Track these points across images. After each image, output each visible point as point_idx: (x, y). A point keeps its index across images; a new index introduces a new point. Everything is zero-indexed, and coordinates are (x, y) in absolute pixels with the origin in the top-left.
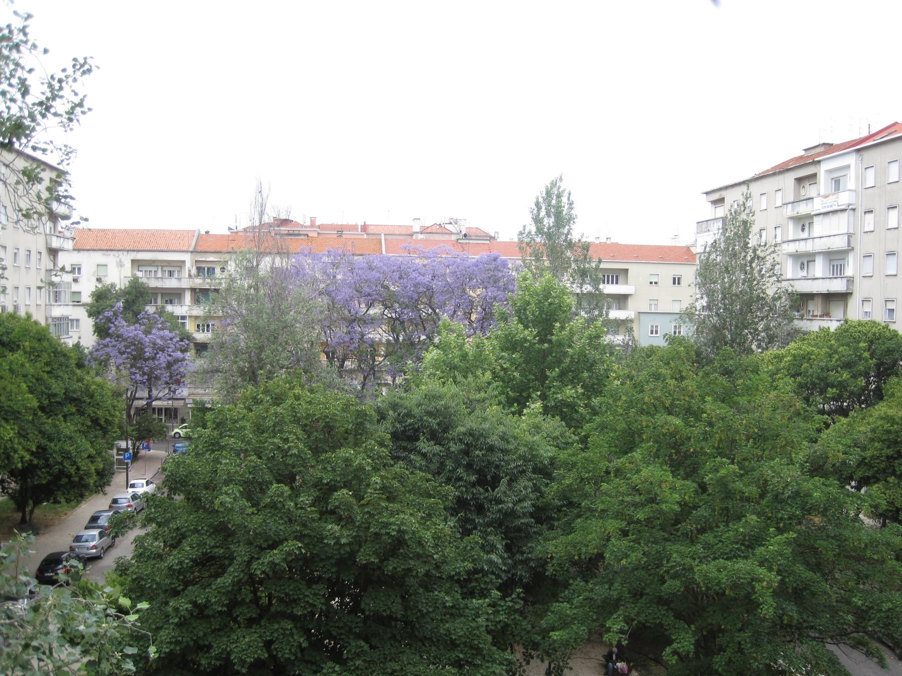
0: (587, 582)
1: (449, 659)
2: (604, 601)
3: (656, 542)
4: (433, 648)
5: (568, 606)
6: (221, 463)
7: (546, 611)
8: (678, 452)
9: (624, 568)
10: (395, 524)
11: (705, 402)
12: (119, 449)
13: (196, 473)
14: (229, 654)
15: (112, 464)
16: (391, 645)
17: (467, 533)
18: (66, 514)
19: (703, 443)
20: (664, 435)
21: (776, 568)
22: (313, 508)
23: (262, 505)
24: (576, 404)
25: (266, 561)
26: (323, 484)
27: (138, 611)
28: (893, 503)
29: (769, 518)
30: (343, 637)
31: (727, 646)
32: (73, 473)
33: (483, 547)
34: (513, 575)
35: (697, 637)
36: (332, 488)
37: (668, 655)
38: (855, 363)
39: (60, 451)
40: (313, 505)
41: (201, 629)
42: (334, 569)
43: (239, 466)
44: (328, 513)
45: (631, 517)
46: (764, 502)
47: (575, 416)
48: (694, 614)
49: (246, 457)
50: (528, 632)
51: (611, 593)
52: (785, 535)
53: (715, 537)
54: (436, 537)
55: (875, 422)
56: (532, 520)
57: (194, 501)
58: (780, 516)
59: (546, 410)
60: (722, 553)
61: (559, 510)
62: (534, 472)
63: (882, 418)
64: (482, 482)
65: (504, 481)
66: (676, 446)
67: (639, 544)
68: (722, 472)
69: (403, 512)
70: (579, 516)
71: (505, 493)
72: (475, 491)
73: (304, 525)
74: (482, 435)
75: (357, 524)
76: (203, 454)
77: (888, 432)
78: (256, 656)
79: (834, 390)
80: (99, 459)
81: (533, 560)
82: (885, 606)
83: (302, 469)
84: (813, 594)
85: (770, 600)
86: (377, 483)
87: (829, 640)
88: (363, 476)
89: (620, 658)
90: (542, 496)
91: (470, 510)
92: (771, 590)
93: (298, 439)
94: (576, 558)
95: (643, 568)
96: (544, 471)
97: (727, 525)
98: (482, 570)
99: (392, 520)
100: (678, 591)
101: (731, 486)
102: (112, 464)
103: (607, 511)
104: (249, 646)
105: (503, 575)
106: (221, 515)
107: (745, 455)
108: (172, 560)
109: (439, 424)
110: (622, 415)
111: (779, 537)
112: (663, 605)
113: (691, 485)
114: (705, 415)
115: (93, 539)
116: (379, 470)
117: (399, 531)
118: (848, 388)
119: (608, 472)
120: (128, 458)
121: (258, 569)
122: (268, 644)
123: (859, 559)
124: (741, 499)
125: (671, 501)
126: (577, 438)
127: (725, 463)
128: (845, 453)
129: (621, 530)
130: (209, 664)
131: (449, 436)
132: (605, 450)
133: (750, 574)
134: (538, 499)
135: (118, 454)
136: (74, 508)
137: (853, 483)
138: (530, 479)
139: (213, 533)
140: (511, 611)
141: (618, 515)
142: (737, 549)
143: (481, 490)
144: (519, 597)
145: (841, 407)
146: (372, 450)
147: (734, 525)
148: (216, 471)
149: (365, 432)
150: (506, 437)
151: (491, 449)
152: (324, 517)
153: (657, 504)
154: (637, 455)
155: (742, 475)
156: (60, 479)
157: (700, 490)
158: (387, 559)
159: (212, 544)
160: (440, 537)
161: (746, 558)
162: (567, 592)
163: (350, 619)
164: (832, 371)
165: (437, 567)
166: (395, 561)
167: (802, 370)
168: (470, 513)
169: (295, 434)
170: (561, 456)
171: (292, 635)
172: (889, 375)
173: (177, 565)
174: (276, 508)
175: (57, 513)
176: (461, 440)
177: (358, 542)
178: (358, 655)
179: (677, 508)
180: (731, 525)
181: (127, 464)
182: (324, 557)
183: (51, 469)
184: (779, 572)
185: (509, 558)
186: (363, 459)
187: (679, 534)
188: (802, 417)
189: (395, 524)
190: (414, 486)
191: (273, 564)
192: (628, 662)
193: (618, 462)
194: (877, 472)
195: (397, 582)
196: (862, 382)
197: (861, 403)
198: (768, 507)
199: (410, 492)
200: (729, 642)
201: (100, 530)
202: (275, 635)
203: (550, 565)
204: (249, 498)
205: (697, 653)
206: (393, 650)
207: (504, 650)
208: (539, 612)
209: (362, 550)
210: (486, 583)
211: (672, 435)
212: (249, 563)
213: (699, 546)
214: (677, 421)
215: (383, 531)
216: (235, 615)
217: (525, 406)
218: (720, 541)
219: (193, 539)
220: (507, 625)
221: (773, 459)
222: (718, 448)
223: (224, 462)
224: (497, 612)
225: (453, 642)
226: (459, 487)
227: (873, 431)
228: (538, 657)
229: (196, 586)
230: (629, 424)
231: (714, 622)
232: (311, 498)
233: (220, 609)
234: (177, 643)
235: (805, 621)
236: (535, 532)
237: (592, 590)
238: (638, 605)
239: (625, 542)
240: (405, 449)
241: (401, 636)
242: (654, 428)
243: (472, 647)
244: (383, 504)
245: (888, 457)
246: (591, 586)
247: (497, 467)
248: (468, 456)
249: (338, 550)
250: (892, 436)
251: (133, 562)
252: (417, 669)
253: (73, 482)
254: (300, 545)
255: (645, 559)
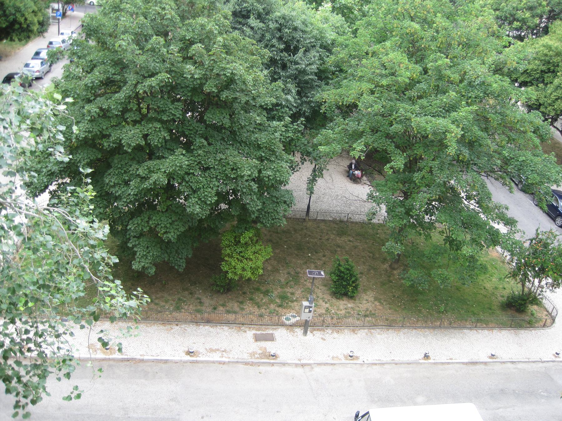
0: (344, 119)
1: (256, 156)
2: (354, 132)
3: (391, 100)
4: (247, 148)
5: (332, 132)
6: (121, 20)
7: (317, 134)
8: (414, 46)
9: (370, 113)
10: (230, 69)
11: (436, 17)
12: (53, 9)
13: (104, 26)
14: (120, 141)
15: (49, 18)
16: (221, 144)
17: (274, 80)
18: (19, 49)
19: (431, 43)
20: (407, 34)
21: (461, 126)
22: (179, 54)
23: (146, 49)
24: (352, 8)
25: (147, 84)
26: (186, 40)
27: (66, 104)
28: (538, 100)
29: (463, 96)
30: (192, 136)
31: (424, 168)
32: (23, 22)
33: (283, 90)
34: (300, 110)
35: (406, 161)
36: (192, 43)
37: (388, 169)
38: (535, 8)
39: (13, 6)
40: (179, 52)
41: (105, 124)
42: (189, 94)
43: (133, 23)
44: (187, 58)
45: (378, 83)
46: (461, 85)
47: (351, 16)
48: (406, 147)
49: (137, 17)
50: (305, 145)
51: (359, 127)
52: (471, 107)
53: (428, 102)
54: (255, 80)
55: (539, 48)
56: (316, 78)
57: (102, 44)
58: (470, 95)
59: (334, 9)
60: (430, 113)
61: (333, 74)
62: (320, 48)
63: (544, 46)
64: (287, 49)
65: (302, 50)
66: (413, 42)
67: (381, 100)
68: (440, 62)
69: (236, 62)
70: (345, 78)
71: (301, 58)
72: (282, 55)
73: (173, 65)
74: (291, 19)
75: (206, 66)
76: (110, 13)
77: (546, 55)
78: (137, 142)
79: (518, 23)
80: (40, 14)
81: (313, 102)
82: (521, 159)
83: (173, 28)
84: (480, 145)
85: (454, 145)
86: (220, 42)
87: (483, 174)
88: (212, 37)
89: (357, 168)
90: (324, 63)
91: (278, 66)
92: (456, 139)
93: (172, 9)
94: (340, 104)
95: (380, 115)
96: (327, 48)
97: (436, 96)
98: (281, 104)
99: (228, 66)
100: (400, 131)
101: (444, 72)
102: (49, 18)
103: (364, 77)
104: (134, 136)
105: (294, 109)
106: (119, 53)
107: (455, 54)
108: (88, 80)
109: (263, 9)
110: (382, 18)
111: (467, 108)
112: (389, 139)
113: (419, 68)
114: (435, 25)
115: (36, 66)
116: (222, 34)
117: (232, 73)
118: (528, 24)
119: (367, 53)
120: (59, 15)
121: (140, 89)
122: (145, 136)
123: (511, 129)
124: (448, 82)
125: (404, 77)
126: (350, 30)
127: (442, 57)
128: (518, 63)
129: (370, 90)
130: (109, 145)
131: (270, 18)
132: (368, 38)
133: (445, 127)
134: (321, 65)
135: (53, 12)
136: (24, 45)
137: (516, 84)
138: (318, 52)
139: (114, 65)
140: (296, 131)
141: (370, 81)
142: (440, 111)
143: (286, 54)
144: (302, 124)
145: (520, 35)
146: (219, 20)
147: (441, 96)
148: (117, 25)
149: (215, 8)
150: (306, 23)
151: (295, 29)
152: (185, 61)
153: (396, 76)
154: (388, 44)
155: (451, 67)
156: (14, 25)
157: (423, 72)
158: (223, 91)
159: (113, 72)
160: (257, 80)
161: (444, 117)
162: (331, 124)
163: (197, 125)
164: (520, 10)
165: (254, 99)
166: (228, 92)
167: (501, 7)
168: (278, 68)
169: (170, 5)
170: (339, 39)
171: (160, 131)
172: (555, 19)
173: (91, 83)
174: (155, 52)
175: (13, 48)
176: (277, 21)
177: (205, 78)
178: (200, 148)
179: (407, 81)
180: (439, 96)
181: (59, 19)
182: (184, 86)
183: (8, 18)
184: (463, 129)
185: (299, 99)
186: (213, 26)
187: (406, 97)
188: (496, 36)
189: (230, 69)
190: (244, 47)
191: (151, 87)
192: (362, 171)
193: (376, 47)
194: (533, 79)
195: (227, 105)
196: (537, 20)
197: (533, 34)
198: (464, 89)
199: (241, 50)
200: (425, 166)
201: (41, 61)
202: (150, 131)
203: (323, 106)
204: (138, 44)
205: (404, 171)
206: (222, 147)
207: (289, 154)
208: (313, 134)
209: (208, 83)
210: (282, 112)
211: (412, 35)
212: (136, 85)
213: (417, 106)
214: (417, 26)
215: (222, 73)
216: (126, 117)
217: (321, 5)
218: (430, 105)
219: (100, 68)
220: (292, 139)
221: (472, 60)
222: (439, 47)
223: (122, 19)
224: (287, 131)
225: (259, 146)
226: (272, 51)
227: (537, 53)
228: (309, 160)
229: (102, 98)
230: (385, 24)
231: (418, 153)
232: (178, 48)
233: (116, 113)
234: (89, 132)
235: (472, 160)
236: (316, 85)
237: (347, 124)
238: (374, 137)
239: (372, 98)
240: (240, 23)
241: (228, 139)
242: (401, 28)
243: (270, 150)
244: (223, 56)
245: (542, 71)
246: (347, 122)
247: (298, 41)
248: (280, 32)
249: (193, 82)
250: (547, 58)
251: (63, 81)
252: (235, 159)
253: (23, 28)
254: (169, 76)
255: (383, 110)
